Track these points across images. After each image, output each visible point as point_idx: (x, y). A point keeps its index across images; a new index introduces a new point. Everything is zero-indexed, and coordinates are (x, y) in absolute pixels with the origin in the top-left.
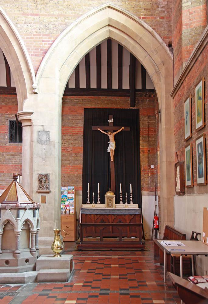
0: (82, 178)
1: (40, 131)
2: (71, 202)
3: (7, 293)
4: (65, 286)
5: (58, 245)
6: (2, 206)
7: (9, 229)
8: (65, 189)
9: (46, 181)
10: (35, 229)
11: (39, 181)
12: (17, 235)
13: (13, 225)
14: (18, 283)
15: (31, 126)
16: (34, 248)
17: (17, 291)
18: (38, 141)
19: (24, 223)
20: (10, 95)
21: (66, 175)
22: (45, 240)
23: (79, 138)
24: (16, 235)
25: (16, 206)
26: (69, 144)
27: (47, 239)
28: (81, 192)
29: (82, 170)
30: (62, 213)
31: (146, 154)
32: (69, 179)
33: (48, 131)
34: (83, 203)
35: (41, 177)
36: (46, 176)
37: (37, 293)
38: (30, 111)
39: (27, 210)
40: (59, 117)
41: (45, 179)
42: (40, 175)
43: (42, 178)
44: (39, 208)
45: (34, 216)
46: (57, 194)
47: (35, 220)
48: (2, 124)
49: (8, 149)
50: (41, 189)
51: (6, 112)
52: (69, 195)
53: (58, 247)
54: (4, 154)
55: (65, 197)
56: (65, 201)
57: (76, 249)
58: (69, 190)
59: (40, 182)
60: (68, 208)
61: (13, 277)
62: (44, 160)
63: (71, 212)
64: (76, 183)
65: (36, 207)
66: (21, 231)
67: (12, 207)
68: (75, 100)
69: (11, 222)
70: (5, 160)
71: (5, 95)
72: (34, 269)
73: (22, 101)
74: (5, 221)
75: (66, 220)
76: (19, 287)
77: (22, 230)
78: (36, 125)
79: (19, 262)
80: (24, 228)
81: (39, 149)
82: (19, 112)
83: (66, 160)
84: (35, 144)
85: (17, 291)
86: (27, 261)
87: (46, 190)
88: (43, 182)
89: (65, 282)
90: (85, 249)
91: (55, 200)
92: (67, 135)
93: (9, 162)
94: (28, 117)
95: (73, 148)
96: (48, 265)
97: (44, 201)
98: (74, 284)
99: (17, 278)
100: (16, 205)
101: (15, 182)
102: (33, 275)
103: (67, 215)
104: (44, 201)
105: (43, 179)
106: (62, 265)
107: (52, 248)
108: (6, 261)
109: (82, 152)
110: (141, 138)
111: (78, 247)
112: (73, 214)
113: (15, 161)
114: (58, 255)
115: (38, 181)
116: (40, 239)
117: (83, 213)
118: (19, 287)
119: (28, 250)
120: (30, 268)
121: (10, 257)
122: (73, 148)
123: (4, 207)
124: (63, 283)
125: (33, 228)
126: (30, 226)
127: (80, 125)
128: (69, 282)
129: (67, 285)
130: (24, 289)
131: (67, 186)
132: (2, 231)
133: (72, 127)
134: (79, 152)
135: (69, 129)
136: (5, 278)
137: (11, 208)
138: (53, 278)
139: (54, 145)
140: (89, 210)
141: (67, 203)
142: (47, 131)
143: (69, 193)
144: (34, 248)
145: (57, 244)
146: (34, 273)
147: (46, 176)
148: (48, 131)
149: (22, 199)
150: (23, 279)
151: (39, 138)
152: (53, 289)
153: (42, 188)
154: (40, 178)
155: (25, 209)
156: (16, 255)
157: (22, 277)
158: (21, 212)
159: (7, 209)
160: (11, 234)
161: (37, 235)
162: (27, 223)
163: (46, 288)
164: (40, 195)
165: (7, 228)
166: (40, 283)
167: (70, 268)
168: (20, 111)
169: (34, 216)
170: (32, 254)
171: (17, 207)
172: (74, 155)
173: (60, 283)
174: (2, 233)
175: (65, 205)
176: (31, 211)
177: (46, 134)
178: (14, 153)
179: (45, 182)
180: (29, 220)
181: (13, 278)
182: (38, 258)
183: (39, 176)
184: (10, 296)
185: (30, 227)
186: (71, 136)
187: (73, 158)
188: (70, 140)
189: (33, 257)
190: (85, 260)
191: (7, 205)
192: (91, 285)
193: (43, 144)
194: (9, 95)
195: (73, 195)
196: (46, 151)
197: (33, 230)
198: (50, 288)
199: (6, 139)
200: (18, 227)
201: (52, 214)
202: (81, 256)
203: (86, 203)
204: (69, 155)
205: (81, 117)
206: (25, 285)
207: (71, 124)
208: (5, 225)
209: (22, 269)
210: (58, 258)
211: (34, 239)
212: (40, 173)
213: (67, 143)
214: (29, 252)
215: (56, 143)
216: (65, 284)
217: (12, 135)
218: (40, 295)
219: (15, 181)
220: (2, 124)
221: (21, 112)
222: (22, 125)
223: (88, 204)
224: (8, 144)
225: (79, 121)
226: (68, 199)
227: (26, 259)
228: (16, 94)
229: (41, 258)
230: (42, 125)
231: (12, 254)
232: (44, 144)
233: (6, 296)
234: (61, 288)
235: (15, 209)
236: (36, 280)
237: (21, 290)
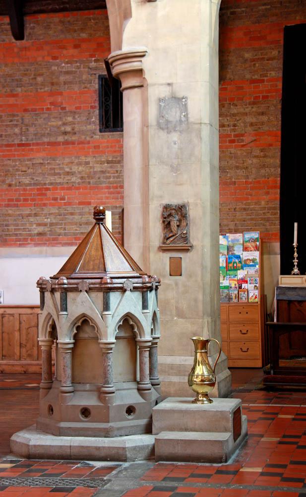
0: (279, 212)
1: (165, 98)
2: (251, 272)
3: (84, 481)
4: (219, 472)
5: (203, 375)
6: (70, 284)
7: (86, 336)
8: (238, 240)
9: (180, 221)
10: (147, 337)
11: (164, 222)
12: (106, 351)
13: (95, 327)
14: (111, 460)
15: (142, 86)
16: (147, 380)
17: (105, 478)
18: (159, 124)
19: (121, 323)
20: (99, 10)
21: (240, 205)
22: (183, 363)
23: (272, 108)
24: (104, 351)
25: (101, 283)
26: (245, 127)
27: (186, 360)
28: (277, 246)
29: (278, 191)
30: (230, 299)
32: (247, 215)
33: (183, 98)
34: (282, 273)
37: (149, 485)
38: (138, 48)
39: (128, 293)
40: (211, 57)
41: (177, 217)
42: (166, 207)
43: (170, 215)
44: (157, 286)
45: (145, 306)
46: (209, 254)
47: (146, 317)
48: (83, 86)
49: (98, 147)
50: (168, 241)
51: (92, 56)
52: (245, 255)
53: (202, 381)
54: (89, 159)
55: (237, 261)
56: (236, 269)
57: (261, 386)
58: (247, 242)
59: (167, 225)
60: (244, 285)
61: (100, 445)
62: (175, 169)
63: (251, 295)
64: (264, 225)
65: (149, 285)
66: (114, 341)
67: (92, 286)
68: (260, 8)
69: (92, 319)
70: (92, 173)
71: (86, 12)
72: (148, 430)
73: (119, 25)
74: (78, 319)
75: (240, 316)
76: (111, 469)
77: (116, 338)
78: (155, 85)
79: (112, 414)
80: (122, 334)
81: (160, 141)
82: (113, 54)
83: (237, 168)
84: (152, 131)
85: (105, 478)
86: (130, 410)
87: (181, 245)
88: (174, 224)
89: (221, 462)
90: (282, 385)
91: (203, 267)
92: (240, 102)
93: (102, 179)
94: (135, 65)
95: (256, 135)
96: (180, 422)
97: (176, 270)
98: (242, 467)
99: (109, 448)
100: (101, 281)
101: (99, 227)
102: (145, 444)
103: (243, 303)
104: (176, 270)
105: (174, 218)
106: (213, 422)
107: (191, 383)
108: (82, 410)
109: (279, 143)
111: (265, 380)
112: (257, 300)
113: (116, 175)
114: (205, 399)
115: (161, 222)
116: (162, 359)
117: (281, 297)
118: (111, 469)
119: (133, 385)
120: (137, 426)
121: (90, 401)
122: (256, 135)
123: (75, 286)
124: (215, 465)
125: (143, 337)
126: (136, 330)
127: (273, 73)
128: (230, 462)
129: (224, 469)
130: (122, 473)
131: (242, 232)
132: (72, 341)
133: (253, 81)
134: (271, 145)
135: (244, 86)
137: (90, 289)
138: (189, 451)
139: (200, 131)
140: (297, 290)
141: (241, 274)
142: (181, 96)
143: (246, 249)
144: (147, 380)
145: (200, 373)
146: (147, 440)
148: (183, 98)
149: (116, 265)
150: (121, 452)
151: (161, 115)
152: (189, 477)
153: (171, 239)
154: (165, 216)
155: (123, 290)
157: (120, 448)
158: (114, 297)
159: (81, 291)
160: (92, 348)
161: (154, 350)
162: (128, 323)
163: (172, 475)
164: (167, 256)
165: (82, 335)
166: (160, 462)
167: (232, 429)
168: (115, 51)
169: (145, 306)
170: (142, 395)
171: (103, 286)
172: (257, 152)
173: (207, 464)
174: (71, 346)
175: (236, 279)
176: (137, 296)
177: (179, 104)
178: (113, 157)
179: (178, 224)
180: (133, 315)
181: (98, 448)
182: (157, 403)
183: (163, 211)
184: (89, 486)
185: (135, 332)
186: (250, 104)
187: (255, 160)
188: (246, 114)
189: (143, 401)
190: (277, 414)
191: (81, 280)
192: (282, 474)
193: (171, 131)
194: (96, 11)
195: (256, 255)
196: (181, 149)
197: (143, 339)
198: (181, 476)
199: (94, 123)
200: (106, 332)
201: (196, 300)
202: (269, 403)
203: (289, 273)
204: (245, 154)
205: (277, 52)
206: (126, 465)
207: (251, 73)
208: (78, 328)
209: (119, 429)
210: (205, 405)
211: (147, 360)
212: (165, 202)
213: (241, 124)
214: (136, 391)
215: (203, 125)
216: (219, 467)
217: (107, 112)
218: (155, 489)
219: (99, 224)
220: (83, 86)
221: (119, 52)
222: (121, 86)
223: (294, 274)
224: (98, 136)
225: (270, 62)
226: (245, 264)
227: (127, 407)
228: (105, 7)
229: (162, 405)
230: (169, 82)
231: (96, 393)
232: (175, 131)
233: (81, 487)
234: (209, 476)
235: (99, 290)
236: (152, 455)
237: (116, 476)
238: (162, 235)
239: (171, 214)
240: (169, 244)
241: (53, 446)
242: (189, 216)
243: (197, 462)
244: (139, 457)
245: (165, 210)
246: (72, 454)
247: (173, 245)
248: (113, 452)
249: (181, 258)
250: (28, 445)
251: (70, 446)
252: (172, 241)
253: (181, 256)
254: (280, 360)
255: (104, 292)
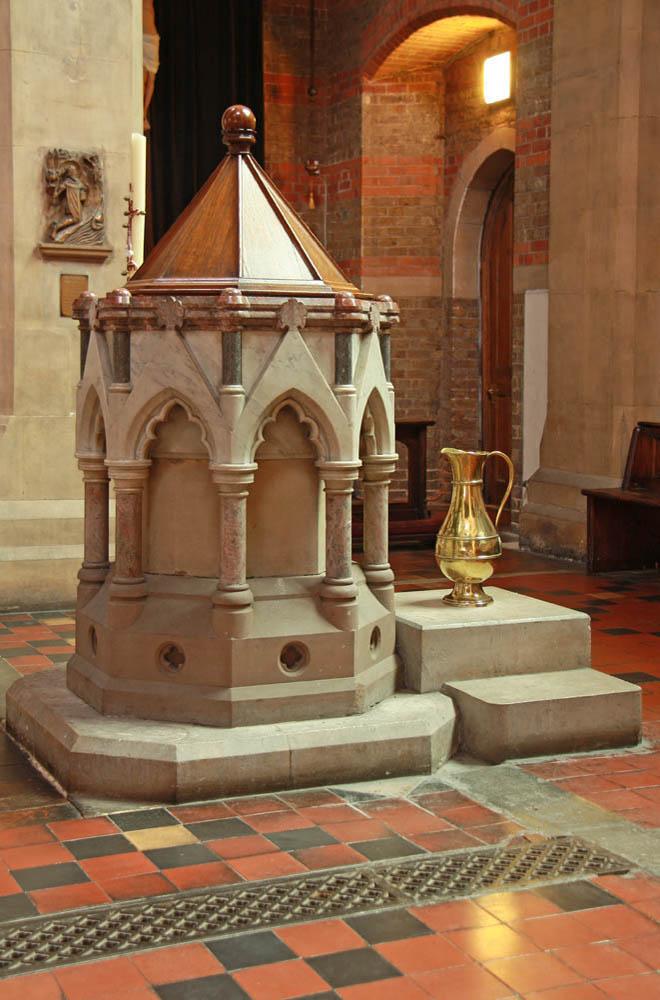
31: (286, 107)
35: (61, 171)
36: (88, 165)
42: (54, 157)
43: (66, 176)
50: (59, 237)
61: (367, 739)
62: (74, 69)
67: (314, 315)
87: (87, 246)
99: (390, 743)
110: (267, 26)
114: (477, 595)
123: (271, 314)
125: (384, 451)
136: (321, 750)
138: (572, 726)
147: (88, 165)
150: (417, 749)
153: (67, 231)
156: (345, 610)
159: (163, 328)
164: (53, 272)
179: (84, 197)
181: (361, 748)
191: (285, 300)
212: (52, 143)
238: (44, 221)
239: (67, 171)
240: (62, 243)
241: (244, 758)
242: (106, 181)
243: (587, 751)
244: (407, 760)
245: (52, 162)
246: (294, 773)
247: (72, 246)
248: (399, 753)
249: (87, 277)
250: (172, 766)
251: (291, 752)
252: (69, 235)
253: (87, 273)
254: (406, 500)
255: (337, 335)
